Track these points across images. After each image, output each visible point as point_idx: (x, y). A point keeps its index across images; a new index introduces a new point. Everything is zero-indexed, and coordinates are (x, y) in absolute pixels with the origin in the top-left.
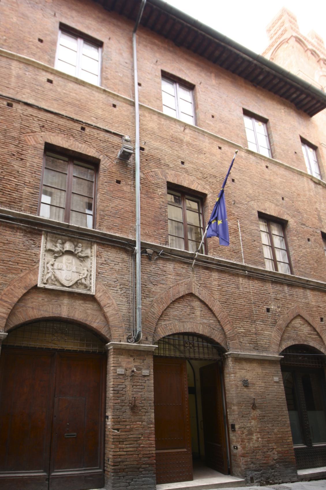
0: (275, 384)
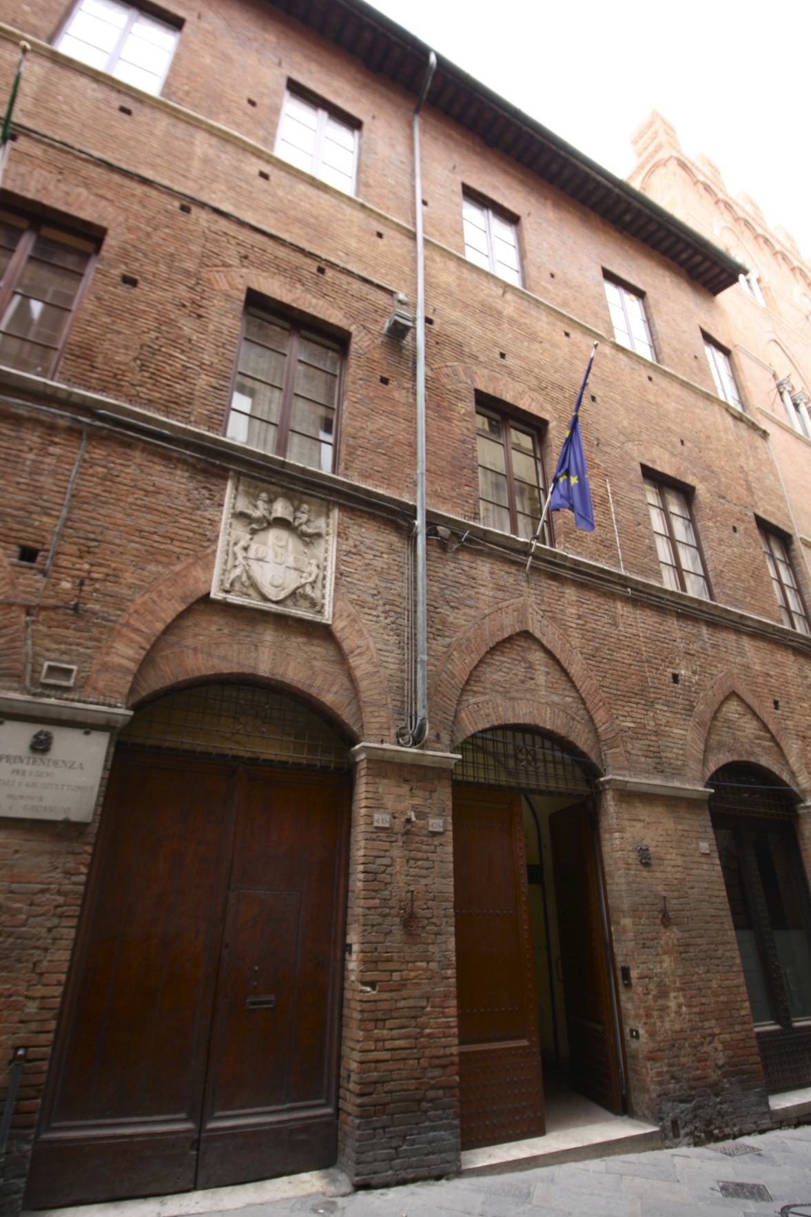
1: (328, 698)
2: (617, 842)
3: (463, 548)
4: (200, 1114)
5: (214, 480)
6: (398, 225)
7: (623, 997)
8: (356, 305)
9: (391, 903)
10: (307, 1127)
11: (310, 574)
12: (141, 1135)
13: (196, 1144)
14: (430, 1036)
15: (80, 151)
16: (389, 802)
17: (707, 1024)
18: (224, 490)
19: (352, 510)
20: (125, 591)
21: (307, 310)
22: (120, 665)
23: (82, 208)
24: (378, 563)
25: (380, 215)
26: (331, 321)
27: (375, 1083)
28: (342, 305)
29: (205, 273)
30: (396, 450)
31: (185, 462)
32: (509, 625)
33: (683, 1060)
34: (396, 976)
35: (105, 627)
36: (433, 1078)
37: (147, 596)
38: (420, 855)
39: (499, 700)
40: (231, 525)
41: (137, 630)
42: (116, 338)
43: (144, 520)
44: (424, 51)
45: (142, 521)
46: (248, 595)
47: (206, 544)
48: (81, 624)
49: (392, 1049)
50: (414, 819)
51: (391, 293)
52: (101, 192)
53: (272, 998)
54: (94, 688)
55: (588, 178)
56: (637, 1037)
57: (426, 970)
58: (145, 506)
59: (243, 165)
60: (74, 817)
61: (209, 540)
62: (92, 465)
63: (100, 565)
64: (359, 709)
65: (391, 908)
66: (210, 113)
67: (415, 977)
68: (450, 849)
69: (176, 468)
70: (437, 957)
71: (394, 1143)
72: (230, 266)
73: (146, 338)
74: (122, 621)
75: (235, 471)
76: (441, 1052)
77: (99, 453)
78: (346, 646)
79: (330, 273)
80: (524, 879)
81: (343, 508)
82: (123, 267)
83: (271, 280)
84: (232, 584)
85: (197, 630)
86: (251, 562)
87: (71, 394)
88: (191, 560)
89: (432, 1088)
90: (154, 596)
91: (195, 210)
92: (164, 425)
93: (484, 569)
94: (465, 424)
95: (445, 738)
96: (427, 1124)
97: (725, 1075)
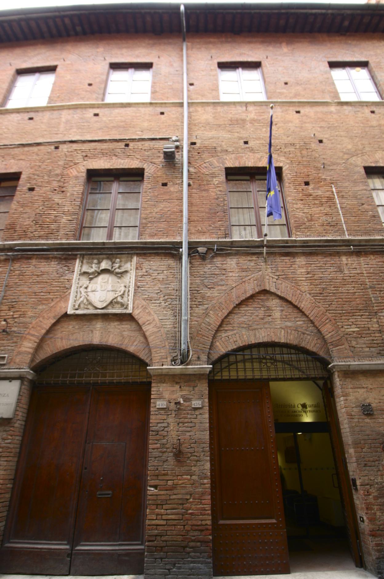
1: (131, 349)
2: (342, 403)
3: (217, 255)
4: (74, 543)
5: (70, 262)
6: (173, 103)
7: (355, 497)
8: (147, 153)
9: (167, 446)
10: (128, 554)
11: (120, 291)
12: (45, 549)
13: (70, 555)
14: (191, 514)
16: (167, 395)
18: (75, 264)
19: (145, 254)
20: (28, 320)
21: (118, 167)
22: (26, 351)
23: (11, 168)
24: (161, 277)
25: (162, 103)
26: (132, 167)
27: (156, 536)
28: (138, 157)
29: (65, 172)
30: (172, 216)
31: (56, 258)
32: (250, 289)
34: (170, 483)
35: (19, 336)
36: (194, 536)
37: (38, 319)
38: (186, 420)
39: (244, 332)
40: (79, 279)
41: (33, 335)
42: (25, 216)
43: (36, 288)
44: (177, 7)
45: (36, 289)
46: (88, 309)
47: (65, 291)
48: (9, 337)
49: (167, 520)
50: (182, 402)
51: (167, 139)
52: (19, 158)
53: (110, 492)
54: (15, 363)
55: (306, 16)
56: (363, 521)
57: (189, 480)
58: (37, 282)
59: (85, 115)
60: (5, 416)
61: (67, 289)
62: (14, 271)
63: (17, 311)
64: (150, 351)
65: (167, 448)
66: (69, 100)
67: (183, 483)
68: (207, 416)
69: (51, 261)
70: (197, 473)
71: (168, 567)
72: (78, 163)
73: (38, 211)
74: (26, 332)
75: (81, 254)
76: (200, 523)
77: (17, 265)
78: (140, 322)
79: (131, 145)
80: (272, 430)
81: (138, 255)
82: (29, 185)
83: (99, 161)
84: (79, 306)
85: (63, 329)
86: (89, 294)
87: (4, 245)
88: (58, 300)
89: (193, 541)
90: (41, 319)
91: (61, 146)
92: (44, 244)
93: (232, 263)
94: (218, 189)
95: (204, 357)
96: (189, 559)
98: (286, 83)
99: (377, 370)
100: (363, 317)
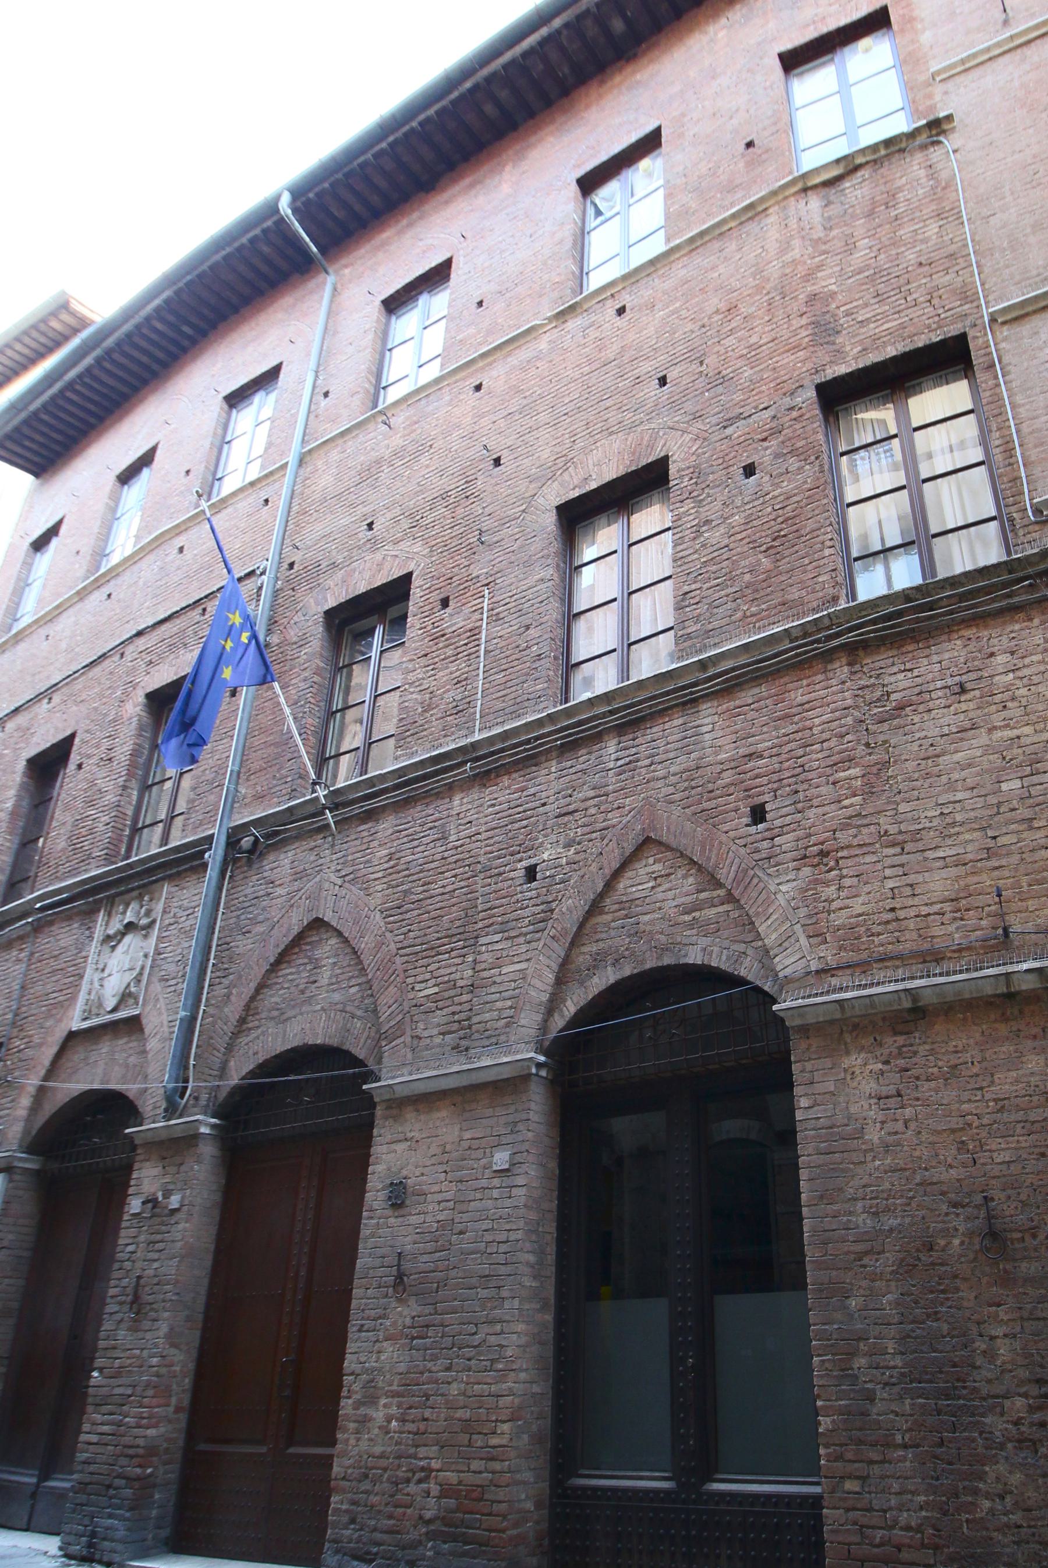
0: (496, 1182)
15: (75, 673)
17: (422, 1452)
33: (374, 1499)
44: (271, 208)
67: (130, 1365)
75: (108, 897)
81: (170, 878)
97: (431, 1536)
98: (480, 304)
99: (440, 1092)
100: (453, 954)
